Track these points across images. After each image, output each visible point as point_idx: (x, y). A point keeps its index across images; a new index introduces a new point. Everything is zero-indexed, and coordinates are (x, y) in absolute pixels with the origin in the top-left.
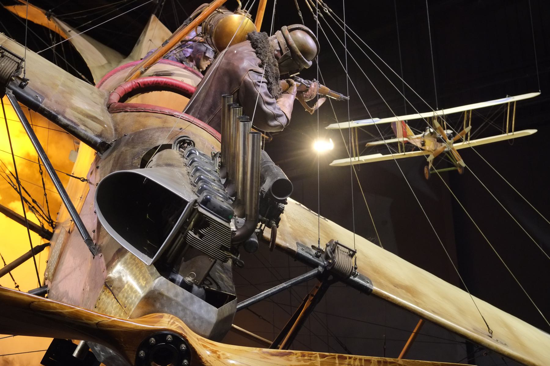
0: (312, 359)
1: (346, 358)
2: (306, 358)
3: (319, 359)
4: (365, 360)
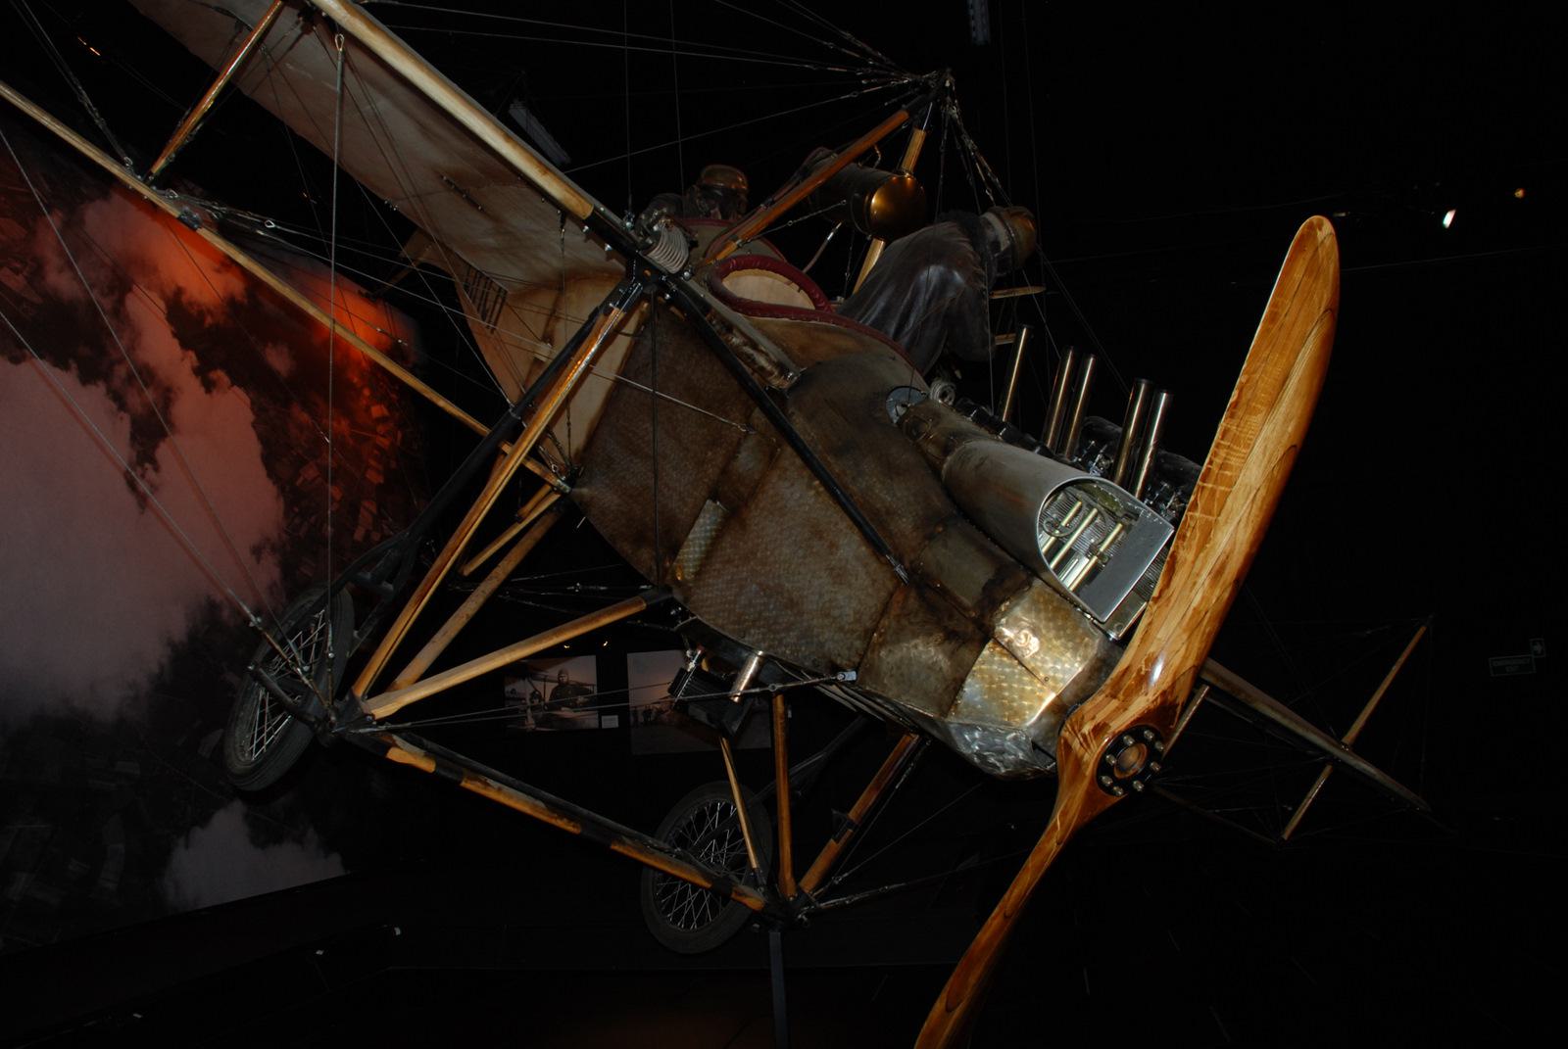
0: (1192, 524)
1: (1208, 470)
2: (1188, 535)
3: (1197, 514)
4: (1222, 439)
